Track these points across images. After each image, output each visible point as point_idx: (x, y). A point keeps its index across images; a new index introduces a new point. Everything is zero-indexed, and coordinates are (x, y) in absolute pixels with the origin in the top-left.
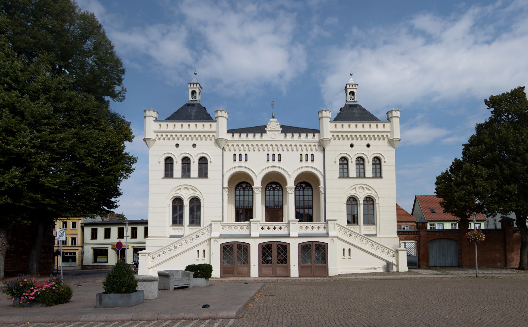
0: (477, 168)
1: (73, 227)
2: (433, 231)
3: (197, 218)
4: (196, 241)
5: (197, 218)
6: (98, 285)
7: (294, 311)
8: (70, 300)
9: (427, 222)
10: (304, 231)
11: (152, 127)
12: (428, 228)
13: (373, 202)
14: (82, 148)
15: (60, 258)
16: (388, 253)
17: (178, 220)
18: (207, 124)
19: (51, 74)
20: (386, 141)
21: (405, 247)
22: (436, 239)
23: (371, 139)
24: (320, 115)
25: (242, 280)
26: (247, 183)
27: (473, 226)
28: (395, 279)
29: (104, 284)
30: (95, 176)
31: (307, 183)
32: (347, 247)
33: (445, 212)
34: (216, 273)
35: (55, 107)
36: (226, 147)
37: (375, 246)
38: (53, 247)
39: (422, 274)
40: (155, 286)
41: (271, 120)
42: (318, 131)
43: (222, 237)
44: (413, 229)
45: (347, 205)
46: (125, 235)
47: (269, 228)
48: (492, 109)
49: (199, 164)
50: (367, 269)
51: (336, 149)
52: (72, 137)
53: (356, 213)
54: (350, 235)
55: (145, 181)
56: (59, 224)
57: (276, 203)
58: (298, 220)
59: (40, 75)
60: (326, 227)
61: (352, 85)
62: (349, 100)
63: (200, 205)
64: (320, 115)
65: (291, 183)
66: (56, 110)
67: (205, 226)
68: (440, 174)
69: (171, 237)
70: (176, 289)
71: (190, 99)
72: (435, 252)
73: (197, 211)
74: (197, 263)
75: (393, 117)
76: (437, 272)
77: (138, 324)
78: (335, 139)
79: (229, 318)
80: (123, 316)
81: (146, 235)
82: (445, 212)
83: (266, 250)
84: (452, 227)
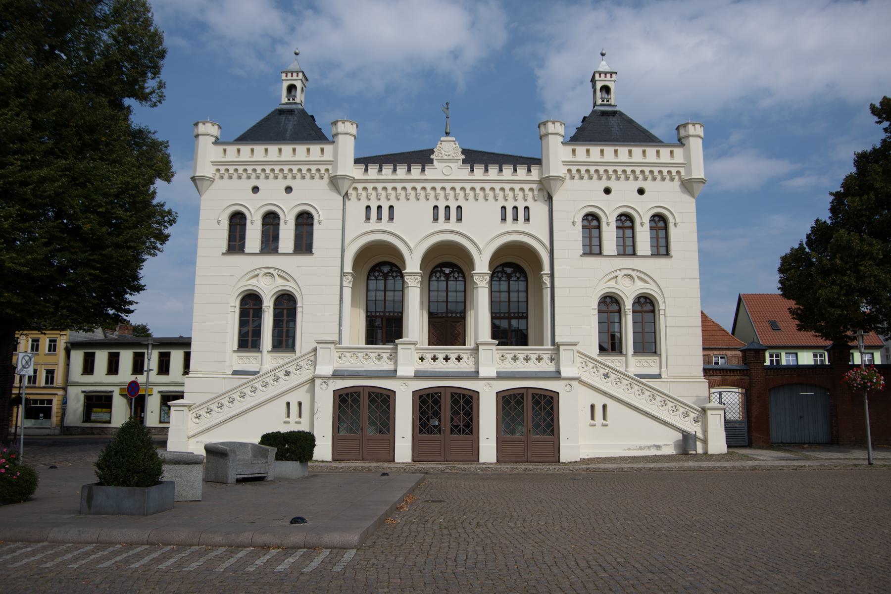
0: (862, 240)
1: (50, 350)
2: (778, 369)
3: (288, 336)
4: (285, 384)
5: (288, 336)
6: (83, 467)
7: (482, 536)
8: (33, 496)
9: (764, 350)
10: (509, 366)
11: (208, 155)
12: (767, 363)
13: (620, 306)
14: (76, 196)
15: (21, 408)
16: (686, 415)
17: (250, 339)
18: (315, 148)
19: (34, 61)
20: (677, 183)
21: (720, 403)
23: (645, 179)
24: (543, 131)
25: (376, 468)
27: (857, 358)
28: (699, 470)
29: (98, 465)
30: (90, 245)
31: (517, 267)
32: (599, 401)
33: (800, 328)
34: (323, 451)
35: (34, 120)
36: (350, 191)
37: (659, 399)
38: (12, 387)
39: (756, 460)
40: (198, 473)
41: (442, 139)
42: (538, 162)
43: (337, 375)
44: (736, 364)
45: (599, 311)
46: (145, 368)
47: (435, 359)
48: (886, 124)
49: (296, 225)
50: (641, 448)
51: (575, 199)
52: (61, 176)
53: (617, 329)
54: (606, 376)
55: (189, 260)
56: (24, 342)
57: (451, 307)
58: (496, 342)
59: (12, 63)
60: (555, 358)
61: (606, 73)
62: (599, 102)
63: (295, 309)
64: (543, 131)
65: (482, 265)
66: (37, 126)
67: (304, 352)
68: (788, 251)
69: (235, 373)
70: (239, 481)
71: (284, 100)
72: (780, 414)
73: (288, 322)
74: (284, 429)
75: (688, 136)
76: (787, 455)
77: (159, 553)
78: (573, 178)
79: (344, 548)
80: (132, 534)
81: (186, 369)
82: (800, 328)
83: (427, 404)
84: (815, 361)
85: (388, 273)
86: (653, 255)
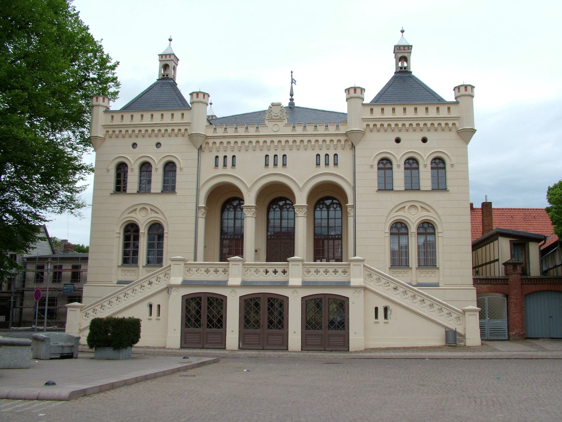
22: (544, 291)
26: (285, 199)
45: (391, 234)
47: (275, 272)
69: (120, 282)
85: (330, 205)
86: (163, 192)
